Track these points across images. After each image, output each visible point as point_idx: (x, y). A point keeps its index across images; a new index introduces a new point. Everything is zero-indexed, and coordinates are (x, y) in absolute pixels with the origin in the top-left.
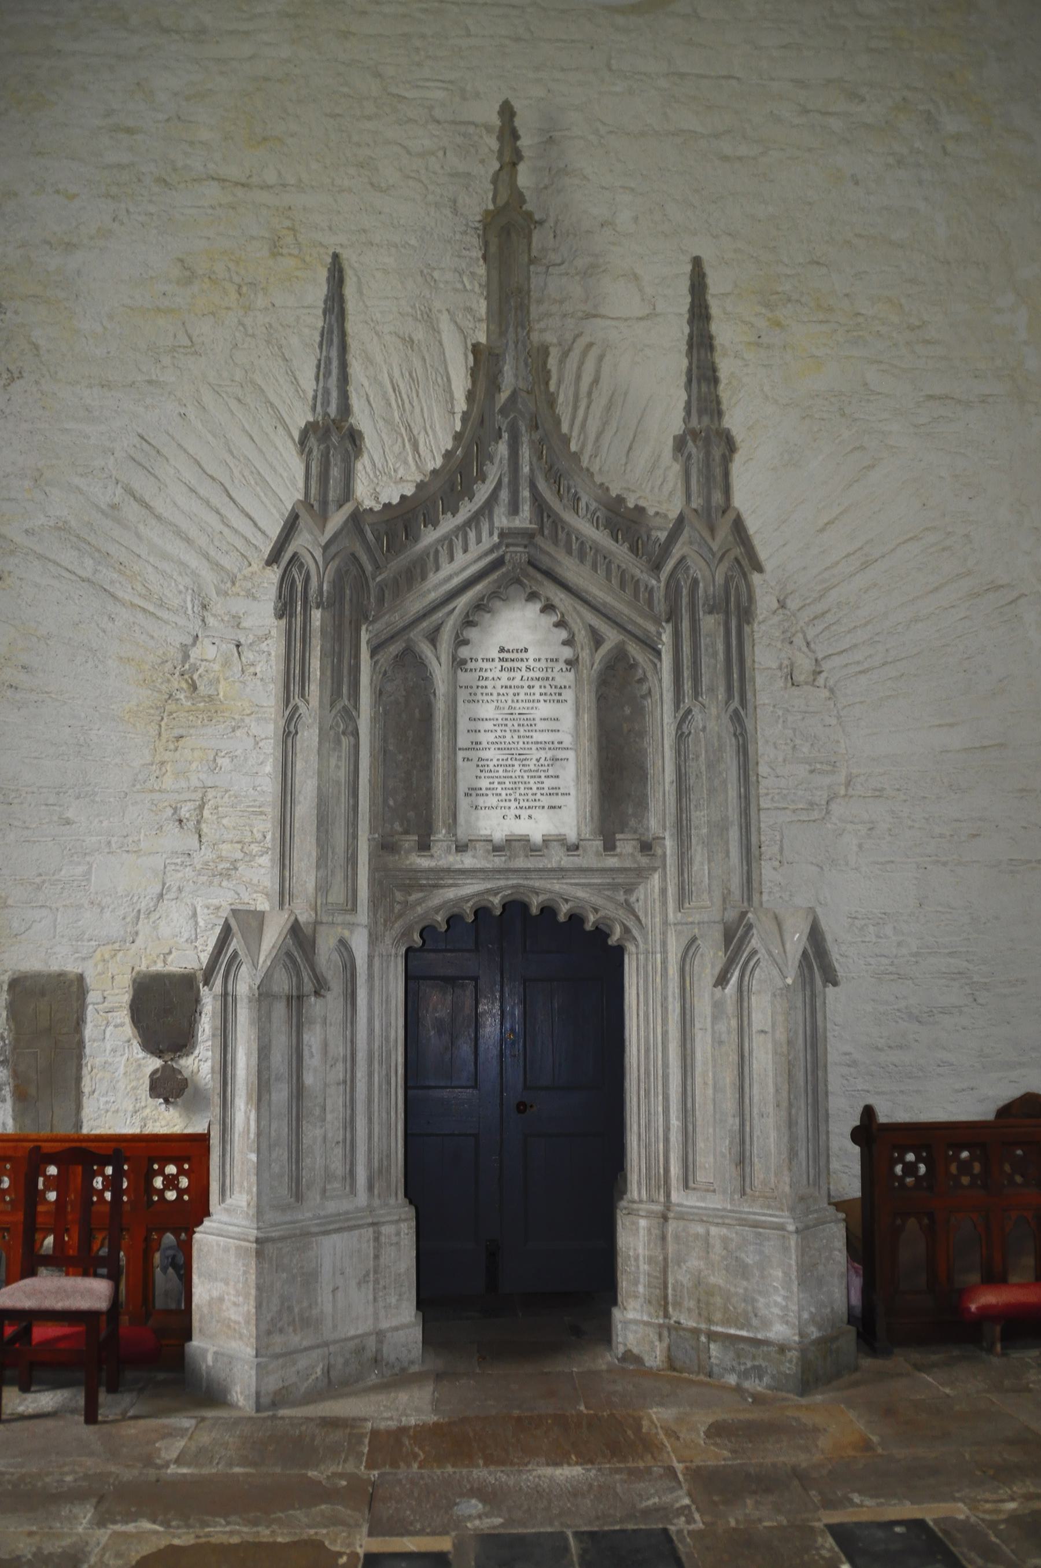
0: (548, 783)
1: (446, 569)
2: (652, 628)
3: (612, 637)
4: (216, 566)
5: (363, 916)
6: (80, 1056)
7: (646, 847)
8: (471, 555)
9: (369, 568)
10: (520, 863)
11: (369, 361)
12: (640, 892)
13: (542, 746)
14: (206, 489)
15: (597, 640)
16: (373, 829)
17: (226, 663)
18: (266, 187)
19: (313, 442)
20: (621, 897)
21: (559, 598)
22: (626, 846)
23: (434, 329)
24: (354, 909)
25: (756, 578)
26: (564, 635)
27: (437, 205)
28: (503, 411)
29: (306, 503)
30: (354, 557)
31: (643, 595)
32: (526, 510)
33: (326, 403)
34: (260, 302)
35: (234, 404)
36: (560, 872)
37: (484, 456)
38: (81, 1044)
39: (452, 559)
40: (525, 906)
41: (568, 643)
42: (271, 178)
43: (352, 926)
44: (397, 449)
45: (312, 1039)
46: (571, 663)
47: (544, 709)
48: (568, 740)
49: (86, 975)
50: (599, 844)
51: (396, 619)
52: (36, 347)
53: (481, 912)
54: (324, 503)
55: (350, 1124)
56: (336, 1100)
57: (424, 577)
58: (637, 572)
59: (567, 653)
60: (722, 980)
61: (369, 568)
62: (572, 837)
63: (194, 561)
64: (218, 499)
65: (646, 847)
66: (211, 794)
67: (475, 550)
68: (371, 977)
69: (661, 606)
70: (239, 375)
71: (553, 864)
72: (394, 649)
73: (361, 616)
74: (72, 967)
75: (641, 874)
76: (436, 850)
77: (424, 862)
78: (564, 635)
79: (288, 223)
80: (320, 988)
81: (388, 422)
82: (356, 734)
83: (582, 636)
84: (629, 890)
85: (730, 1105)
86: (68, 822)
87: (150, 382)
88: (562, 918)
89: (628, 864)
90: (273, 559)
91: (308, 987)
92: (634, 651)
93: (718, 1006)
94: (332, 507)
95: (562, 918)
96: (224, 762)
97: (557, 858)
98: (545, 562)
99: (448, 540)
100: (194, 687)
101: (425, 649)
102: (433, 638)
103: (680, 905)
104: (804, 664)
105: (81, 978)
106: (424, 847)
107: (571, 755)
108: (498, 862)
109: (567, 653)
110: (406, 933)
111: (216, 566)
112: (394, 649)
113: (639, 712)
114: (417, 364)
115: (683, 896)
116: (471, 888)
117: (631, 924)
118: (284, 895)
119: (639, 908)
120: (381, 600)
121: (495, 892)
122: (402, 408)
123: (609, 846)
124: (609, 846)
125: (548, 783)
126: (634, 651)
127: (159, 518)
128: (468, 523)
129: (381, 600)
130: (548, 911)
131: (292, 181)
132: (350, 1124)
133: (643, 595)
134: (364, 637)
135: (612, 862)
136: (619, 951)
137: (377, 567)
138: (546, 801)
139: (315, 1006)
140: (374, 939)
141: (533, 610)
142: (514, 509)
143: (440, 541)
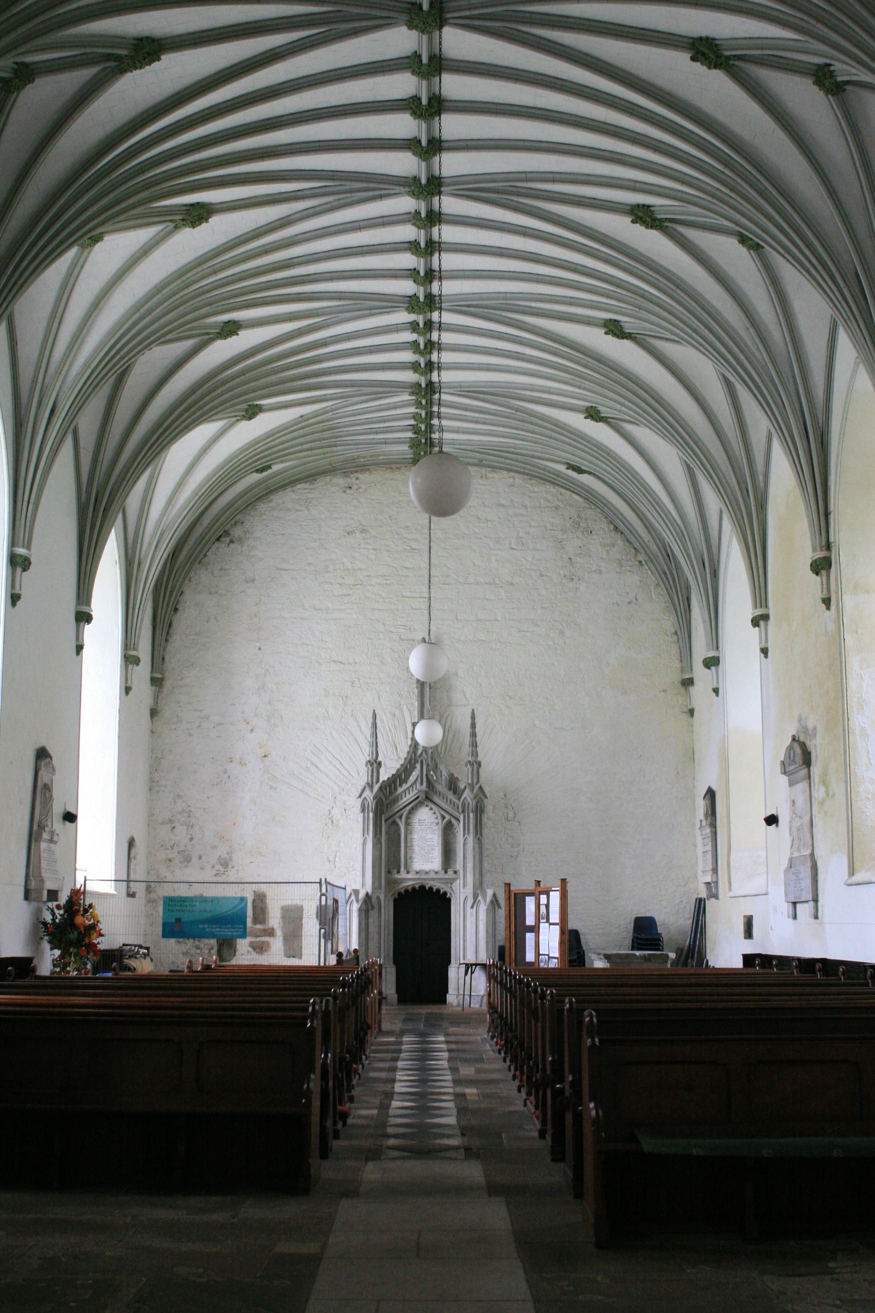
0: (431, 856)
1: (404, 799)
2: (457, 814)
3: (448, 817)
4: (339, 786)
5: (383, 890)
6: (302, 928)
7: (455, 872)
8: (410, 796)
9: (384, 799)
10: (423, 877)
11: (382, 721)
12: (454, 884)
13: (429, 846)
14: (335, 762)
15: (443, 817)
16: (385, 867)
17: (342, 815)
18: (350, 664)
19: (369, 766)
20: (449, 885)
21: (433, 806)
22: (450, 872)
23: (402, 711)
24: (381, 888)
25: (485, 801)
26: (435, 816)
27: (402, 669)
28: (419, 757)
29: (368, 784)
30: (380, 798)
31: (456, 806)
32: (425, 784)
33: (372, 755)
34: (349, 702)
35: (342, 735)
36: (433, 879)
37: (413, 768)
38: (302, 925)
39: (406, 796)
40: (425, 887)
41: (437, 818)
42: (351, 660)
43: (380, 893)
44: (391, 749)
45: (371, 920)
46: (437, 824)
47: (430, 836)
48: (436, 844)
49: (304, 906)
50: (443, 872)
51: (389, 814)
52: (282, 717)
53: (414, 889)
54: (372, 783)
55: (379, 942)
56: (376, 937)
57: (398, 801)
58: (454, 800)
59: (436, 821)
60: (472, 907)
61: (384, 799)
62: (436, 870)
63: (331, 784)
64: (338, 766)
65: (455, 872)
66: (338, 853)
67: (412, 794)
68: (385, 906)
69: (460, 810)
70: (343, 726)
71: (431, 877)
72: (391, 820)
73: (382, 812)
74: (299, 903)
75: (454, 880)
76: (401, 873)
77: (398, 876)
78: (435, 816)
79: (357, 676)
80: (373, 908)
81: (388, 741)
82: (381, 843)
83: (439, 817)
84: (452, 884)
85: (474, 939)
86: (297, 861)
87: (316, 728)
88: (441, 893)
89: (451, 877)
90: (360, 796)
91: (370, 908)
92: (453, 821)
93: (471, 914)
94: (374, 784)
95: (441, 893)
96: (342, 844)
97: (432, 875)
98: (430, 797)
99: (405, 791)
100: (333, 822)
101: (398, 821)
102: (401, 817)
103: (464, 887)
104: (511, 815)
105: (302, 906)
106: (398, 872)
107: (437, 848)
108: (417, 876)
109: (436, 821)
110: (394, 894)
111: (339, 786)
112: (391, 820)
113: (455, 836)
114: (397, 723)
115: (464, 885)
116: (410, 883)
117: (452, 892)
118: (363, 885)
119: (454, 888)
120: (387, 807)
121: (417, 884)
122: (392, 737)
123: (446, 872)
124: (446, 872)
125: (431, 856)
126: (453, 821)
127: (321, 771)
128: (410, 787)
129: (387, 807)
130: (431, 888)
131: (358, 662)
132: (379, 942)
133: (456, 806)
134: (383, 818)
135: (447, 876)
136: (449, 900)
137: (386, 799)
138: (430, 860)
139: (371, 913)
140: (386, 896)
141: (427, 809)
142: (422, 784)
143: (403, 792)
